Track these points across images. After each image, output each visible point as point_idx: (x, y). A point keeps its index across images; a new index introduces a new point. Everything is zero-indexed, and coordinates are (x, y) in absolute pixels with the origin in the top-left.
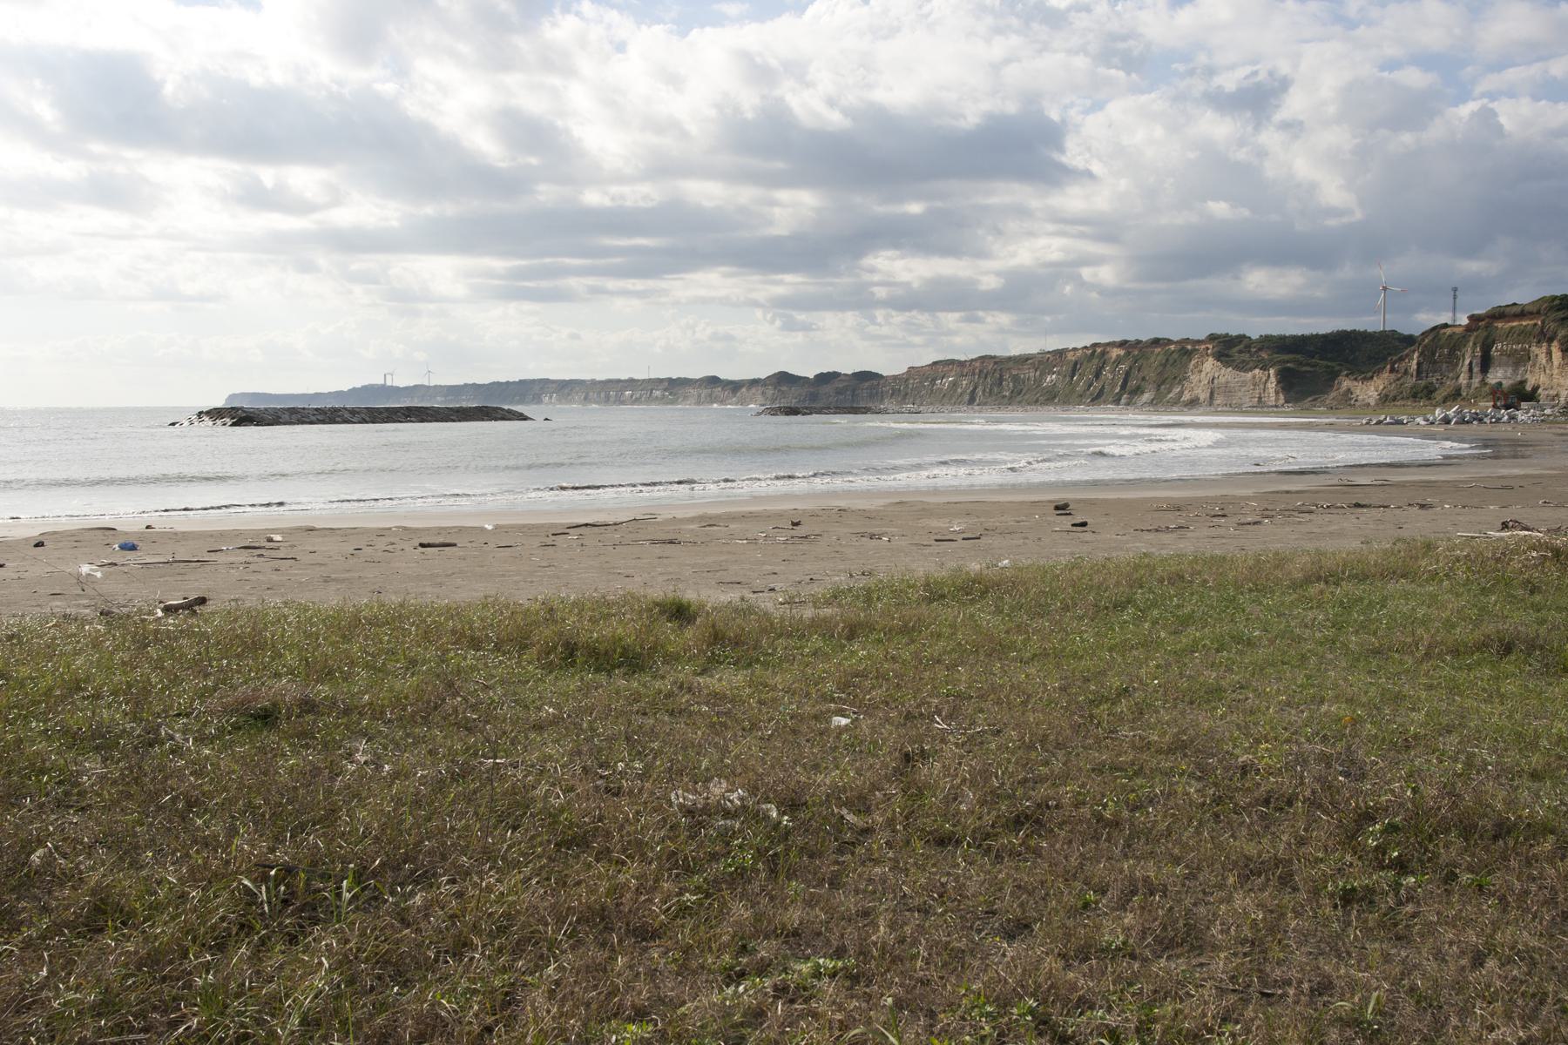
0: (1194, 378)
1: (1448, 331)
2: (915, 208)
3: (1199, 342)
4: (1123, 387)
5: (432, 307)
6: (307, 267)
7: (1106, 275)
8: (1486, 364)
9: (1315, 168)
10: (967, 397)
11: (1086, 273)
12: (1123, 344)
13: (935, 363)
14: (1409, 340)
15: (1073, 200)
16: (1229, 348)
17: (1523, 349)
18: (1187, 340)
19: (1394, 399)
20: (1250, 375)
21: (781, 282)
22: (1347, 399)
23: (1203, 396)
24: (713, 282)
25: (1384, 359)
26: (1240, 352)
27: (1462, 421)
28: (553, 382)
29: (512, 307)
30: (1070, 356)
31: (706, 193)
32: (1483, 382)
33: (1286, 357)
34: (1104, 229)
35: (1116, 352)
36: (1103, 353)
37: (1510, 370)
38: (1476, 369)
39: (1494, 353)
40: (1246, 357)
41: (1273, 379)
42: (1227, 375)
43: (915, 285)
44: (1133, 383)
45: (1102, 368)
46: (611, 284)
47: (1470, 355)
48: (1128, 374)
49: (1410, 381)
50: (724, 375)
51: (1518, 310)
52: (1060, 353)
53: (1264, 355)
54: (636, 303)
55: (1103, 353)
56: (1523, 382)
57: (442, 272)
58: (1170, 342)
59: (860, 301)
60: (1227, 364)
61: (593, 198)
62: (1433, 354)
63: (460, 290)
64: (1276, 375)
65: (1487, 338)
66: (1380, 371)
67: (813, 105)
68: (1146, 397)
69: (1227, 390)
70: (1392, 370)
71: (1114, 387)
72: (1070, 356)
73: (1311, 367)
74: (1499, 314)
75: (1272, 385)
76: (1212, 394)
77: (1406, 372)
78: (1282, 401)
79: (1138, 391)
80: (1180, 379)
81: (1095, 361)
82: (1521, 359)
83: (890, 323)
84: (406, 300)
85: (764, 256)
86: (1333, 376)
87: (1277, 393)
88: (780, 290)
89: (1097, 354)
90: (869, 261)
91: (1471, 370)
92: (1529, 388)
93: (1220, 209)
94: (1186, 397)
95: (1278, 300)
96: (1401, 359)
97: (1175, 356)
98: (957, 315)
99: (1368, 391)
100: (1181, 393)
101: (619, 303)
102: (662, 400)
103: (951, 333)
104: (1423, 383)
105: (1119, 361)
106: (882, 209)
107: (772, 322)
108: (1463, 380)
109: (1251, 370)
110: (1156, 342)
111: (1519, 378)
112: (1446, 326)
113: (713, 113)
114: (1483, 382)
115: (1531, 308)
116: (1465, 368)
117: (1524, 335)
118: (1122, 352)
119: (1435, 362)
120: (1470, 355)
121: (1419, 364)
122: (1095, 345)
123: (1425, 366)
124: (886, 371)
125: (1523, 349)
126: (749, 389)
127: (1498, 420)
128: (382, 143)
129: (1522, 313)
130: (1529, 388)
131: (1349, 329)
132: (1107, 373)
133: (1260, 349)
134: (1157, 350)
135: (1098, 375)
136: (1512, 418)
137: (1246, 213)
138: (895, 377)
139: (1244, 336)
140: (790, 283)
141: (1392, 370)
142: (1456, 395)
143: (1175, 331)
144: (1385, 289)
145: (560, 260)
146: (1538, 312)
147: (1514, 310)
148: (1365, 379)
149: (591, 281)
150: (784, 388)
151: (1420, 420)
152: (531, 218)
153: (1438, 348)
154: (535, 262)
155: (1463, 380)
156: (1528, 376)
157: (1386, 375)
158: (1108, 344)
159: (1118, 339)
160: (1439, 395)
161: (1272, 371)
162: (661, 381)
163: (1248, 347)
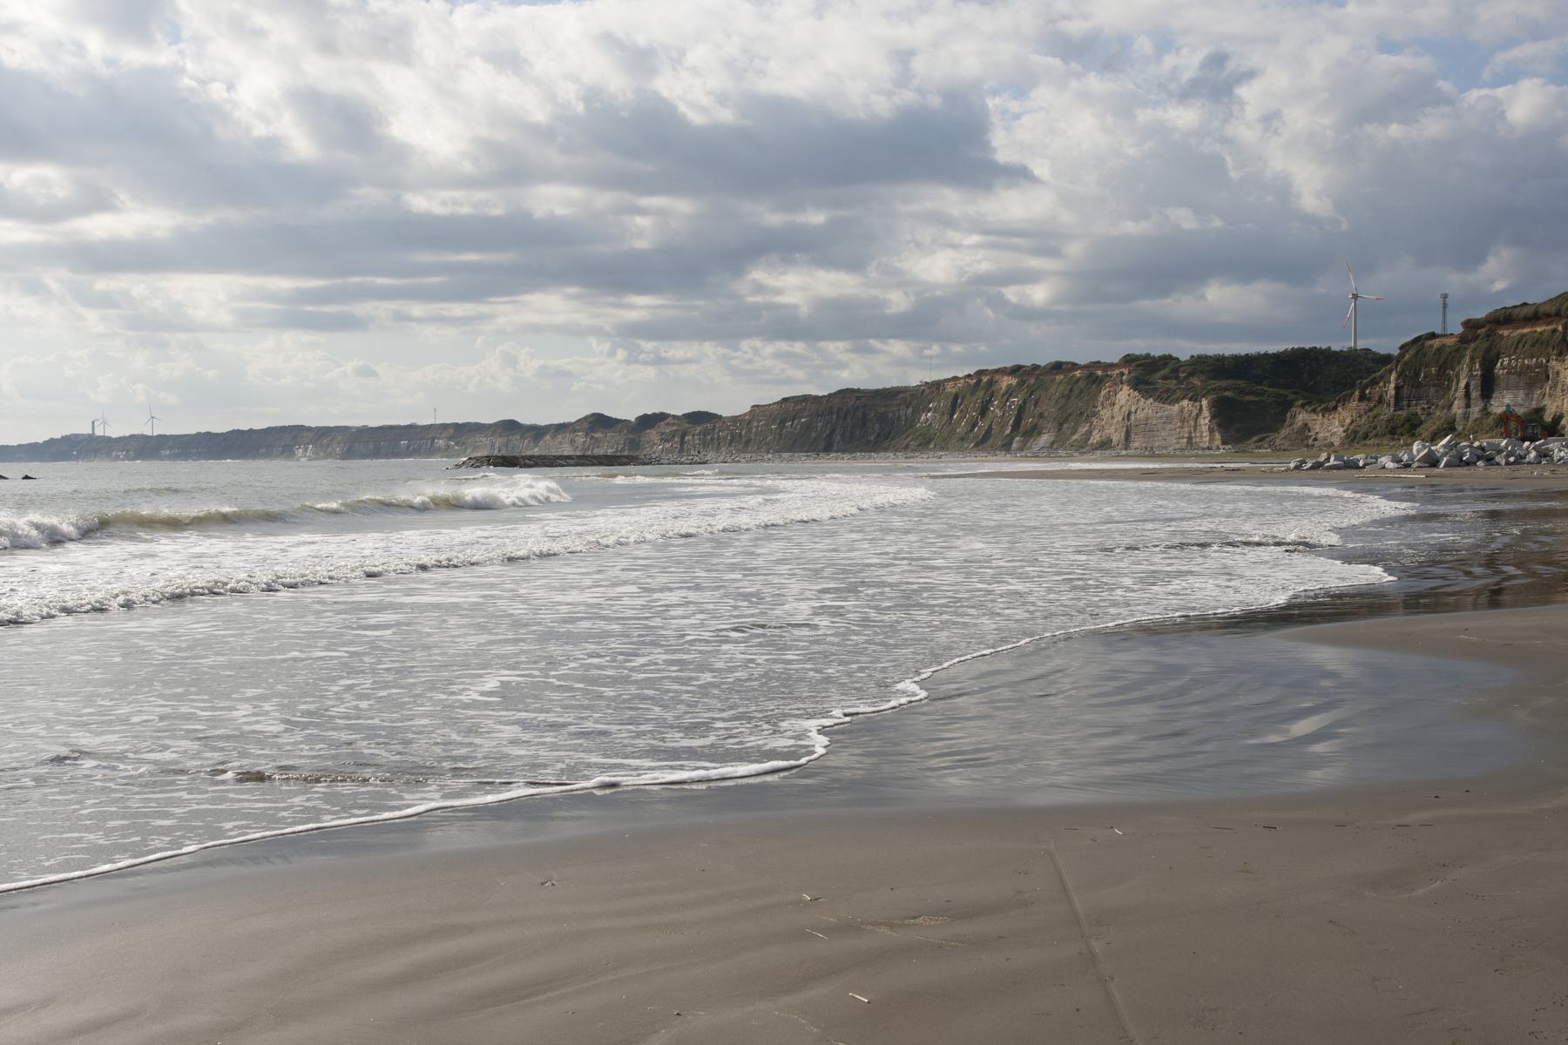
0: (1105, 413)
1: (1436, 343)
2: (817, 218)
3: (1112, 366)
4: (1016, 426)
5: (184, 337)
6: (33, 288)
7: (1039, 294)
8: (1488, 386)
9: (1293, 156)
10: (822, 444)
11: (1011, 293)
12: (1016, 370)
13: (785, 400)
14: (1386, 359)
15: (1013, 206)
16: (1149, 374)
17: (1539, 365)
18: (1097, 364)
19: (1366, 436)
20: (1176, 408)
21: (631, 307)
22: (1303, 438)
23: (1117, 437)
24: (553, 305)
25: (1353, 386)
26: (1165, 378)
27: (1458, 462)
28: (309, 429)
29: (289, 337)
30: (950, 388)
31: (553, 200)
32: (1485, 412)
33: (1224, 383)
34: (1044, 239)
35: (1006, 382)
36: (991, 383)
37: (1521, 394)
38: (1475, 394)
39: (1499, 370)
40: (1172, 384)
41: (1206, 413)
42: (1147, 408)
43: (804, 310)
44: (1028, 421)
45: (990, 402)
46: (417, 310)
47: (1465, 375)
48: (1021, 411)
49: (1387, 412)
50: (525, 420)
51: (1531, 311)
52: (937, 385)
53: (1196, 382)
54: (451, 332)
55: (991, 383)
56: (1540, 411)
57: (207, 294)
58: (1074, 366)
59: (733, 326)
60: (1146, 394)
61: (420, 203)
62: (1417, 375)
63: (225, 318)
64: (1212, 405)
65: (1489, 349)
66: (1345, 400)
67: (695, 93)
68: (1045, 439)
69: (1148, 429)
70: (1362, 398)
71: (1003, 427)
72: (950, 388)
73: (1260, 400)
74: (1504, 318)
75: (1205, 421)
76: (1128, 434)
77: (1381, 400)
78: (1218, 442)
79: (1034, 431)
80: (1088, 415)
81: (980, 393)
82: (1538, 378)
83: (763, 353)
84: (153, 327)
85: (607, 273)
86: (1285, 406)
87: (1211, 431)
88: (633, 316)
89: (982, 383)
90: (758, 275)
91: (1467, 395)
92: (1548, 418)
93: (1185, 219)
94: (1096, 438)
95: (1236, 315)
96: (1374, 383)
97: (1081, 384)
98: (841, 345)
99: (1332, 427)
100: (1089, 433)
101: (429, 331)
102: (175, 457)
103: (841, 366)
104: (1403, 414)
105: (1010, 393)
106: (774, 219)
107: (612, 353)
108: (1457, 409)
109: (1177, 401)
110: (1058, 367)
111: (1534, 405)
112: (1433, 336)
113: (580, 108)
114: (1485, 412)
115: (1548, 309)
116: (1461, 392)
117: (1538, 345)
118: (1014, 381)
119: (1419, 386)
120: (1465, 375)
121: (1397, 388)
122: (980, 373)
123: (1405, 391)
124: (726, 411)
125: (1539, 365)
126: (554, 437)
127: (1520, 459)
128: (150, 135)
129: (1535, 315)
130: (1548, 418)
131: (1307, 346)
132: (995, 409)
133: (1191, 374)
134: (1060, 377)
135: (983, 412)
136: (1544, 454)
137: (1218, 223)
138: (735, 419)
139: (1170, 357)
140: (641, 306)
141: (1362, 398)
142: (1449, 427)
143: (1082, 352)
144: (1355, 297)
145: (370, 279)
146: (1558, 314)
147: (1525, 310)
148: (1326, 411)
149: (394, 306)
150: (598, 435)
151: (1386, 461)
152: (331, 225)
153: (1424, 365)
154: (339, 281)
155: (1457, 409)
156: (1546, 401)
157: (1354, 404)
158: (997, 371)
159: (1009, 364)
160: (1428, 427)
161: (1204, 402)
162: (445, 426)
163: (1175, 371)
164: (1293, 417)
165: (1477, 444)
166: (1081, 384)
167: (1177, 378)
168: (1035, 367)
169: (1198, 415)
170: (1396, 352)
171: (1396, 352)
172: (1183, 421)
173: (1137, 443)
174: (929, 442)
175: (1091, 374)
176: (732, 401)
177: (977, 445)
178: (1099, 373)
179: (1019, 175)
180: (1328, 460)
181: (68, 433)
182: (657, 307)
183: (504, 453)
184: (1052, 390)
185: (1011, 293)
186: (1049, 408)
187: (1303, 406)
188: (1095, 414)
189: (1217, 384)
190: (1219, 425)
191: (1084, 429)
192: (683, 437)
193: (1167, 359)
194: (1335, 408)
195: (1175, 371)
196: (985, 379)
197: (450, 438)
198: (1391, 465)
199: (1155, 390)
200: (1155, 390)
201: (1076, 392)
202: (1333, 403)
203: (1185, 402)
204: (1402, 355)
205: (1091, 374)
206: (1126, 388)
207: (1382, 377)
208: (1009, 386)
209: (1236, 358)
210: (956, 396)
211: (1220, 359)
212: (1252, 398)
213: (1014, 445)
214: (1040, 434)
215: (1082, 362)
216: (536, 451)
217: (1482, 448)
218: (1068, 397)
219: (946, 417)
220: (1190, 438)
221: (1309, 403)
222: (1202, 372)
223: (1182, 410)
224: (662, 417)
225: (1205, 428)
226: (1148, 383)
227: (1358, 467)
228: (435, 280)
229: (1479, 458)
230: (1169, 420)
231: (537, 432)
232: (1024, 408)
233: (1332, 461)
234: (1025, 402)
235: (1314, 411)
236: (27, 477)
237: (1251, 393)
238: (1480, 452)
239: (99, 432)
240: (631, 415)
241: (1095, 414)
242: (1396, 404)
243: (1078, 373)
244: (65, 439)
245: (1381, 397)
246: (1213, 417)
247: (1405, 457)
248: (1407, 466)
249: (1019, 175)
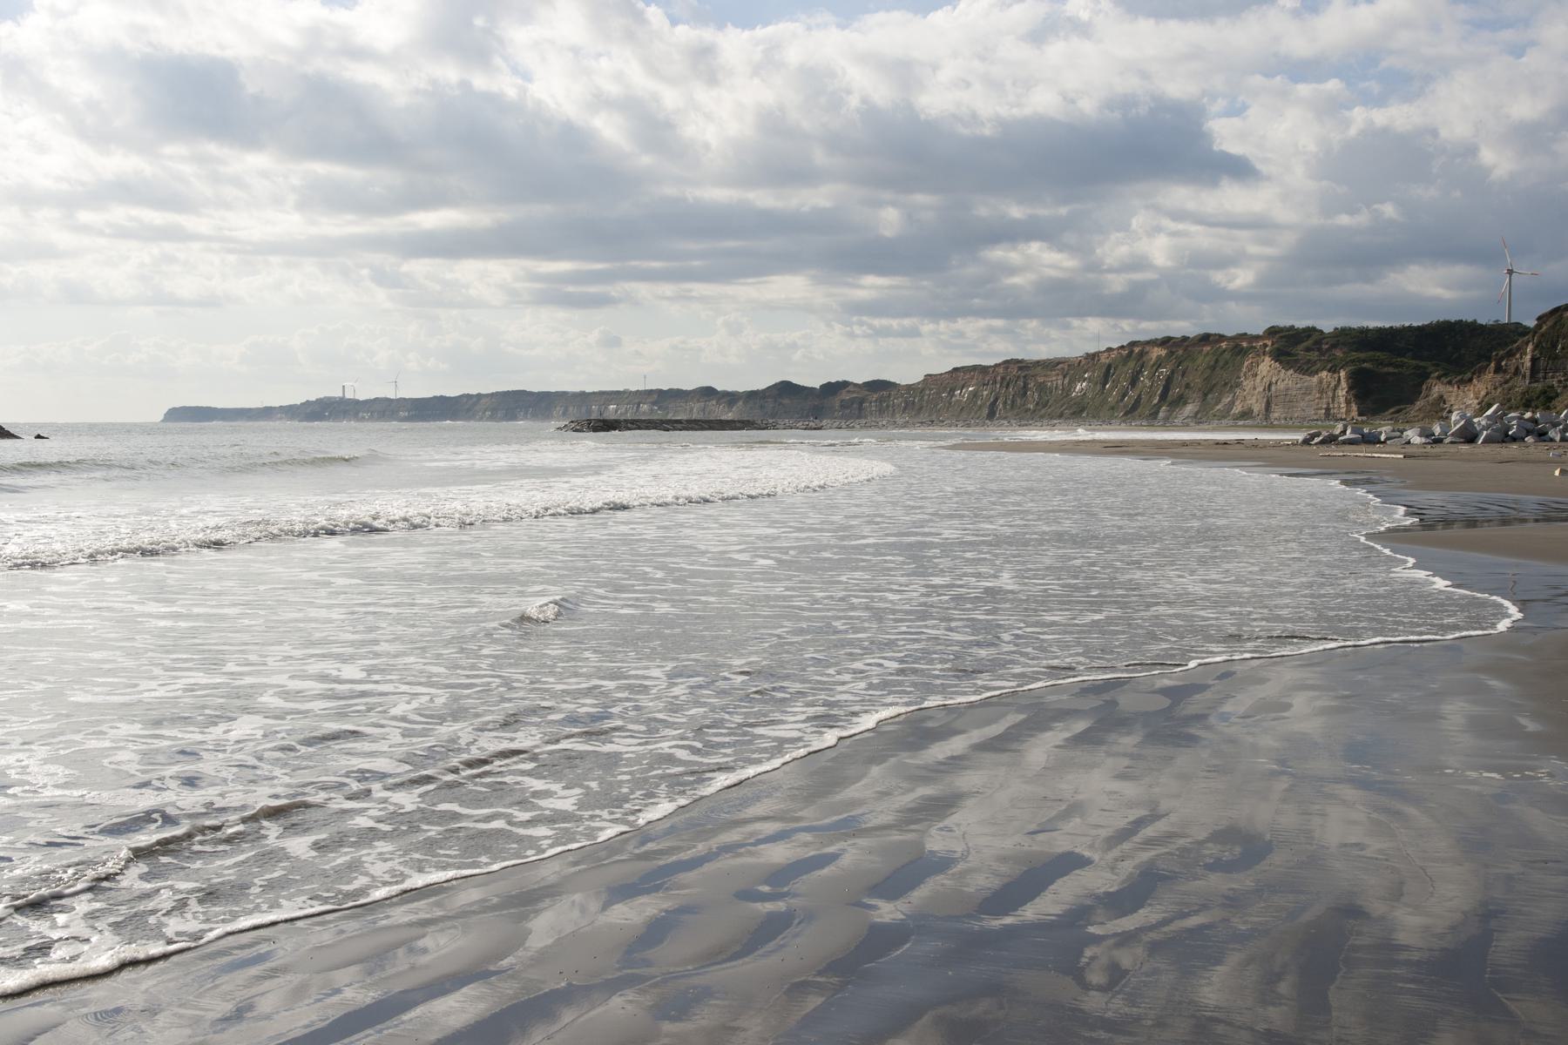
0: (1247, 384)
3: (1257, 338)
4: (1163, 397)
10: (986, 411)
12: (1166, 342)
13: (956, 370)
16: (1291, 345)
18: (1243, 336)
20: (1315, 379)
24: (792, 286)
25: (1489, 359)
26: (1308, 350)
27: (1504, 438)
28: (531, 393)
30: (1104, 360)
33: (1362, 355)
34: (1257, 224)
40: (1314, 355)
41: (1344, 384)
42: (1287, 380)
45: (1140, 372)
48: (1169, 381)
49: (1522, 384)
53: (1339, 353)
55: (1142, 354)
58: (1221, 338)
62: (1554, 346)
64: (1350, 377)
66: (1481, 371)
68: (1190, 409)
69: (1289, 402)
70: (1498, 370)
75: (1342, 392)
78: (1354, 413)
79: (1181, 401)
81: (1131, 364)
87: (1348, 402)
88: (861, 294)
94: (1238, 408)
96: (1510, 354)
97: (1227, 356)
100: (1232, 403)
104: (1539, 386)
105: (1159, 363)
106: (1016, 212)
110: (1205, 338)
118: (1163, 352)
119: (1556, 357)
121: (1534, 360)
122: (1133, 344)
123: (1542, 363)
133: (1334, 346)
134: (1207, 349)
135: (1134, 382)
138: (909, 387)
139: (1314, 329)
140: (871, 286)
141: (1498, 370)
148: (1462, 382)
150: (786, 401)
157: (1489, 376)
158: (1148, 343)
161: (1342, 374)
163: (1318, 343)
164: (1429, 389)
165: (1528, 415)
166: (1227, 356)
167: (1319, 350)
168: (1185, 339)
169: (1336, 387)
170: (1531, 323)
171: (1531, 323)
172: (1321, 392)
173: (1276, 413)
174: (1082, 411)
175: (1237, 346)
176: (906, 373)
177: (1126, 414)
178: (1245, 344)
179: (1239, 169)
180: (1344, 432)
181: (381, 395)
182: (890, 287)
183: (700, 417)
184: (1199, 361)
185: (1218, 277)
186: (1196, 380)
187: (1439, 378)
188: (1238, 385)
189: (1355, 355)
190: (1356, 396)
191: (1226, 400)
192: (861, 404)
193: (1310, 331)
194: (1471, 380)
195: (1318, 343)
196: (1137, 350)
197: (654, 403)
198: (1417, 440)
199: (1297, 361)
200: (1297, 361)
201: (1221, 363)
202: (1468, 375)
203: (1324, 373)
204: (1539, 327)
205: (1237, 346)
206: (1267, 359)
207: (1518, 349)
208: (1159, 357)
209: (1380, 330)
210: (1109, 367)
211: (1364, 332)
212: (1391, 370)
213: (1161, 415)
214: (1185, 403)
215: (1229, 334)
216: (730, 416)
217: (1535, 421)
218: (1213, 368)
219: (1099, 387)
220: (1328, 409)
221: (1445, 375)
222: (1344, 344)
223: (1321, 382)
224: (845, 384)
225: (1342, 400)
226: (1289, 354)
227: (1380, 442)
228: (696, 263)
229: (1529, 433)
230: (1308, 391)
231: (731, 398)
232: (1170, 378)
233: (1349, 435)
234: (1173, 372)
235: (1450, 383)
236: (39, 437)
237: (1390, 364)
238: (1530, 426)
239: (349, 396)
240: (816, 383)
241: (1238, 385)
242: (1532, 376)
243: (1224, 345)
244: (319, 401)
245: (1517, 369)
246: (1350, 388)
247: (1437, 430)
248: (1439, 441)
249: (1239, 169)
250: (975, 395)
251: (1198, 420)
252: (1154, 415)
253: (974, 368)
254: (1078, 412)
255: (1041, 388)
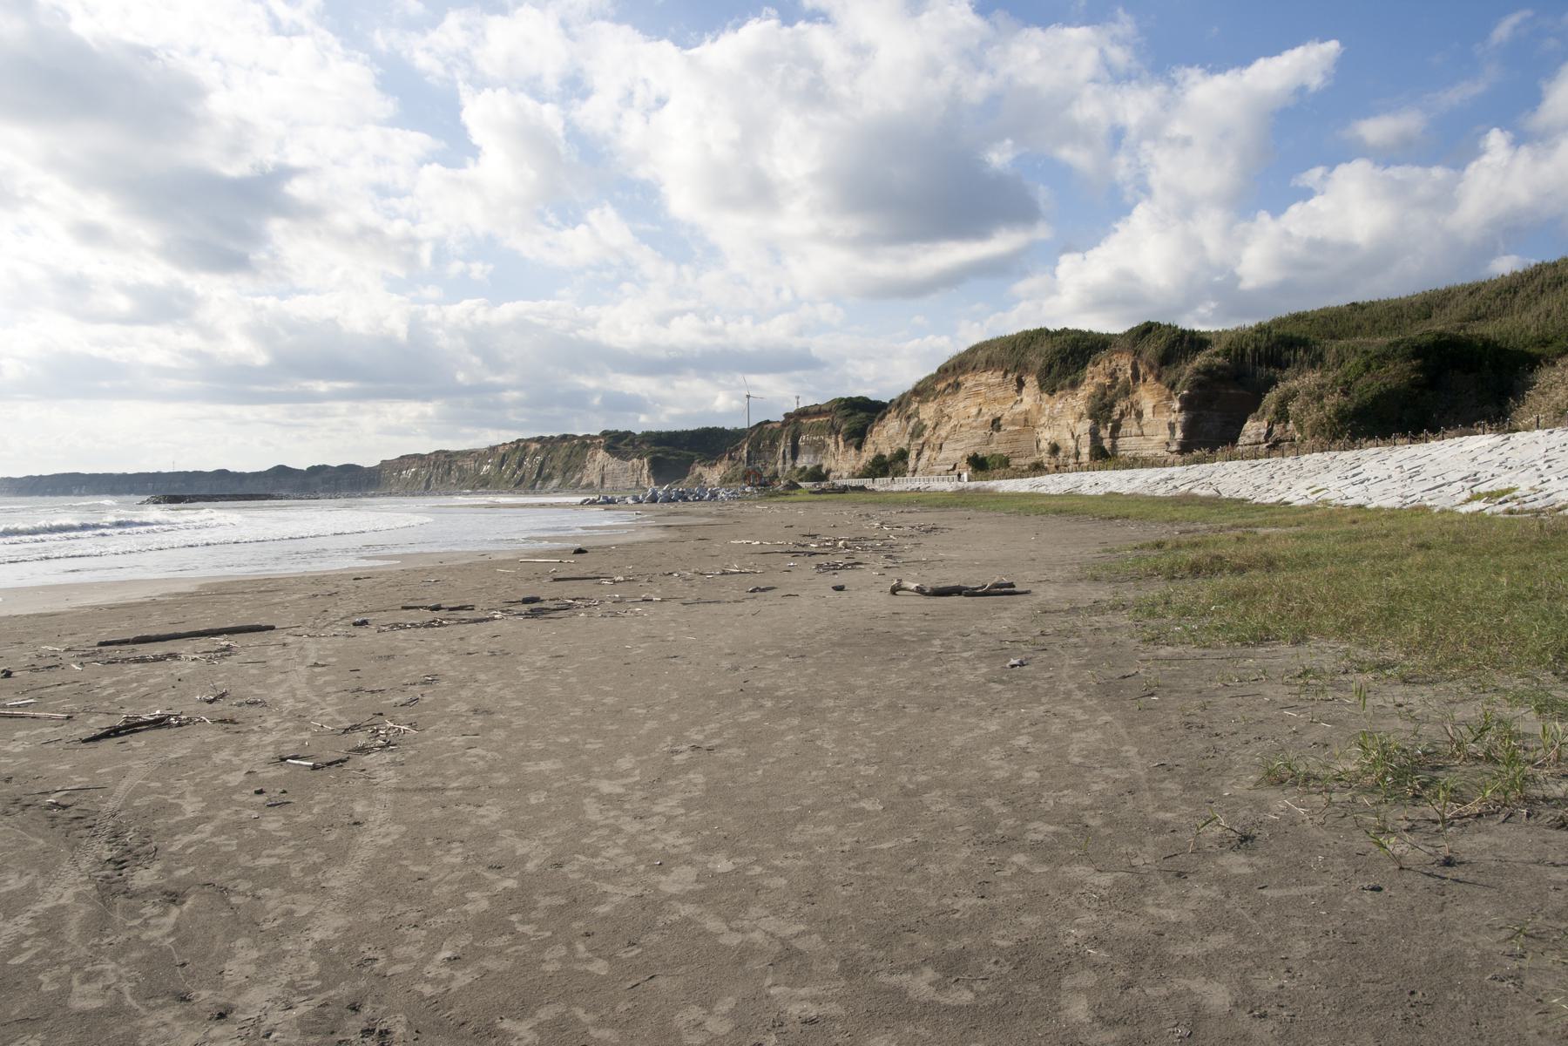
0: (589, 466)
4: (539, 474)
30: (501, 451)
42: (613, 464)
49: (742, 467)
55: (525, 447)
58: (574, 437)
68: (555, 482)
79: (550, 477)
105: (536, 453)
110: (564, 438)
135: (520, 465)
157: (725, 461)
230: (626, 471)
250: (416, 474)
251: (557, 491)
252: (533, 487)
253: (415, 456)
254: (483, 484)
255: (460, 469)
